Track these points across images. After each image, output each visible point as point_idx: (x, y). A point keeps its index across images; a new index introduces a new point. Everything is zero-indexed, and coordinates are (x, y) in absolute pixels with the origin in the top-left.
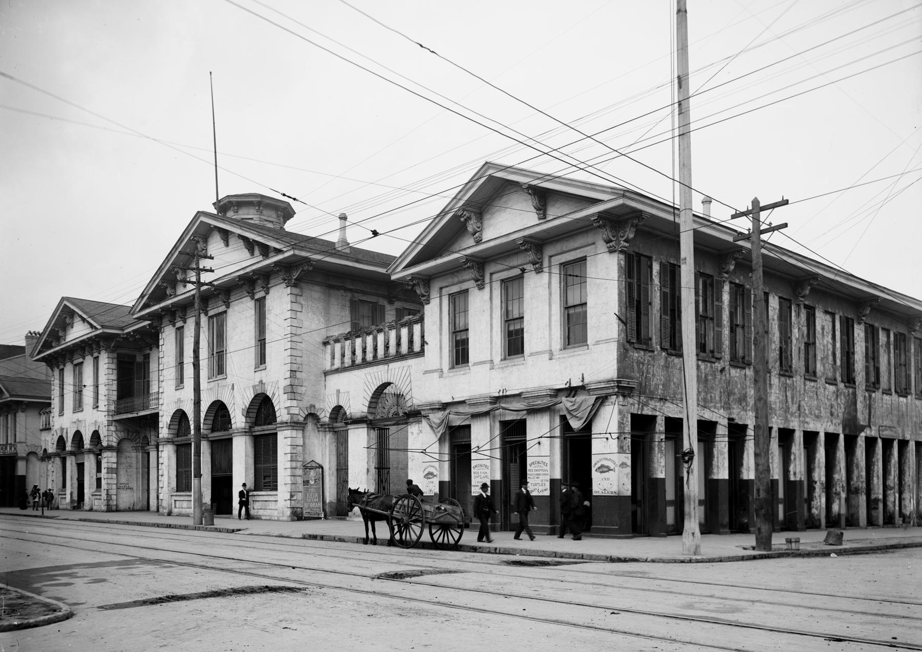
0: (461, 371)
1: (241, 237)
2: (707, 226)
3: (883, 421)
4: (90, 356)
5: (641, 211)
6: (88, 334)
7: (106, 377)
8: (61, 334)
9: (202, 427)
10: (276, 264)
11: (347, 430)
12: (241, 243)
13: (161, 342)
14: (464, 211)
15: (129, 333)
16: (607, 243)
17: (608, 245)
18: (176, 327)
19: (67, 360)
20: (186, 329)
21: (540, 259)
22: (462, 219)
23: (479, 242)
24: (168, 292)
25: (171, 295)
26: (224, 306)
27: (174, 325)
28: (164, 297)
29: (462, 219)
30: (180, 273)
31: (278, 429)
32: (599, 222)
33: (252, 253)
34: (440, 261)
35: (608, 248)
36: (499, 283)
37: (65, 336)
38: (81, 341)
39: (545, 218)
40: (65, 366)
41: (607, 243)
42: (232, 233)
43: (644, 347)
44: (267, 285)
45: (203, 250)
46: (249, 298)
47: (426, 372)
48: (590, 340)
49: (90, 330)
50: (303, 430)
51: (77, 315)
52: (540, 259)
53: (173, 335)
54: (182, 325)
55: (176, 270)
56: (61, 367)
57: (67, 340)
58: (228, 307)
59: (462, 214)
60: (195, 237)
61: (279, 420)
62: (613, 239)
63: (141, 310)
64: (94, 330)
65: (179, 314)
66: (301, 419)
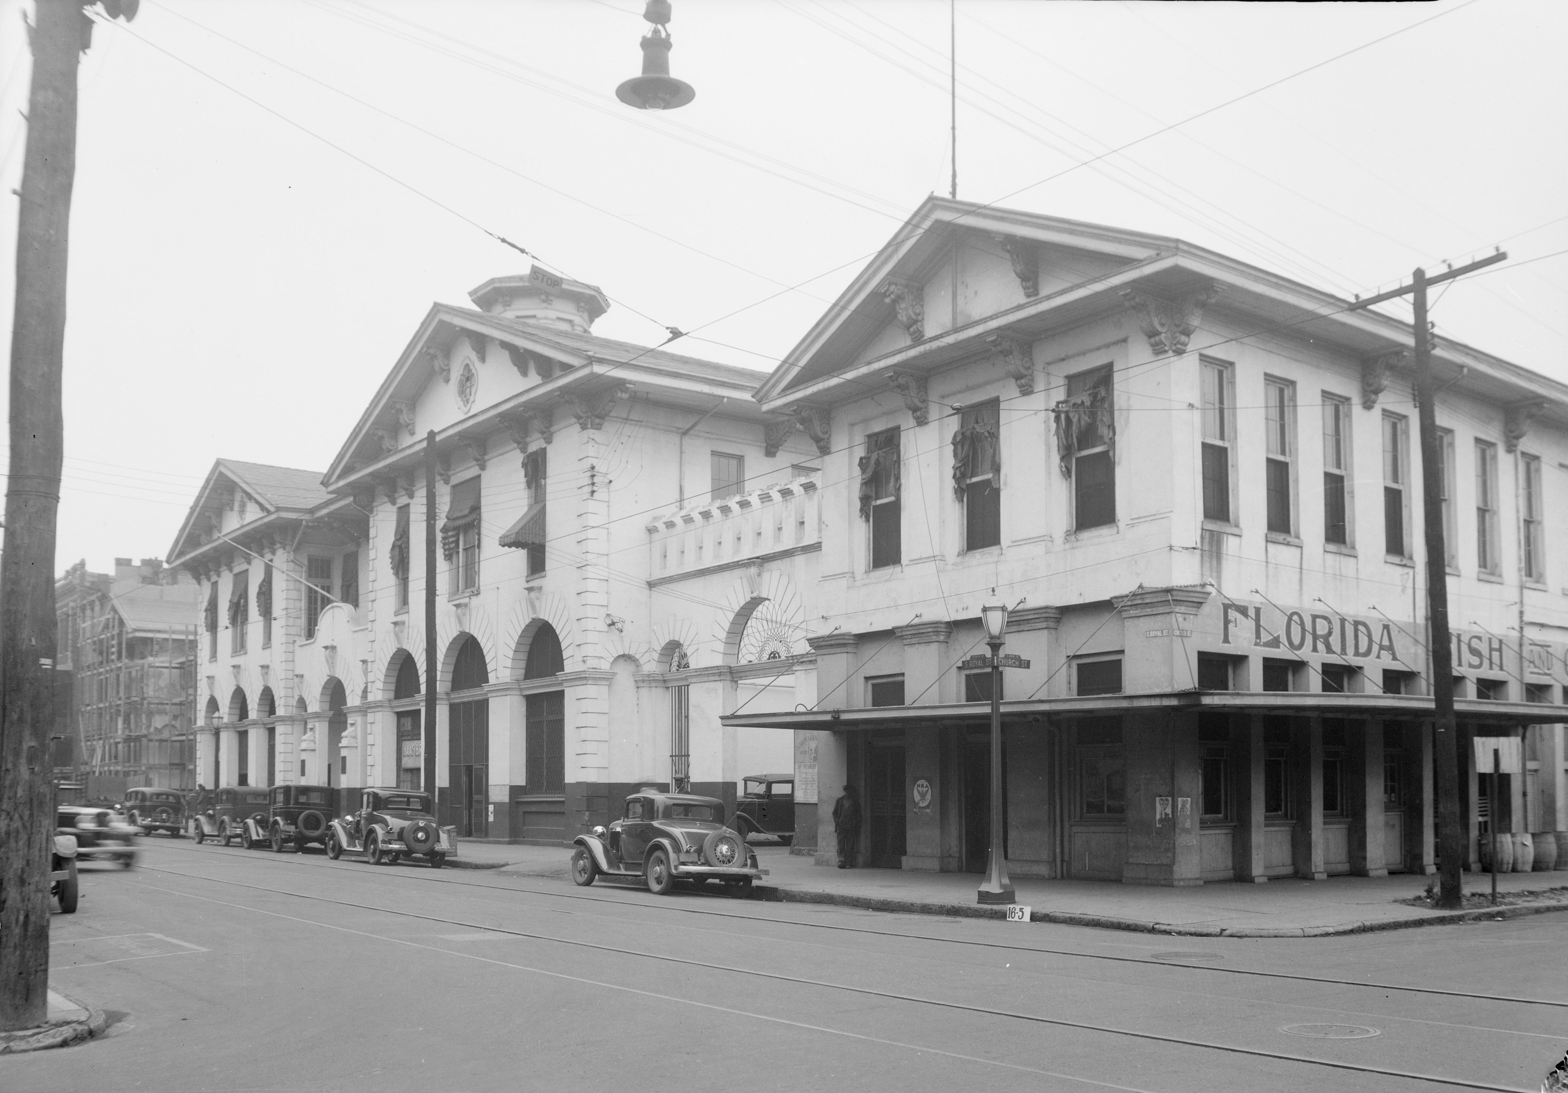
0: (982, 557)
1: (505, 345)
2: (1331, 304)
3: (148, 759)
4: (389, 505)
5: (1211, 279)
6: (256, 520)
7: (284, 595)
8: (404, 418)
9: (438, 678)
10: (564, 390)
11: (688, 686)
12: (506, 354)
13: (372, 532)
14: (890, 284)
15: (322, 517)
16: (1150, 337)
17: (1153, 340)
18: (398, 505)
19: (224, 568)
20: (412, 509)
21: (1029, 368)
22: (887, 300)
23: (918, 339)
24: (387, 444)
25: (389, 451)
26: (477, 468)
27: (393, 503)
28: (198, 545)
29: (887, 300)
30: (405, 412)
31: (565, 685)
32: (1133, 298)
33: (524, 373)
34: (850, 375)
35: (1020, 387)
36: (1062, 381)
37: (220, 523)
38: (459, 434)
39: (1037, 294)
40: (219, 576)
41: (1150, 337)
42: (492, 339)
43: (193, 704)
44: (548, 427)
45: (444, 370)
46: (518, 451)
47: (826, 578)
48: (905, 558)
49: (534, 378)
50: (609, 686)
51: (239, 490)
52: (1029, 368)
53: (394, 517)
54: (406, 502)
55: (398, 406)
56: (214, 578)
57: (224, 532)
58: (483, 467)
59: (888, 290)
60: (428, 348)
61: (569, 666)
62: (1159, 328)
63: (340, 477)
64: (265, 514)
65: (536, 424)
66: (605, 666)
